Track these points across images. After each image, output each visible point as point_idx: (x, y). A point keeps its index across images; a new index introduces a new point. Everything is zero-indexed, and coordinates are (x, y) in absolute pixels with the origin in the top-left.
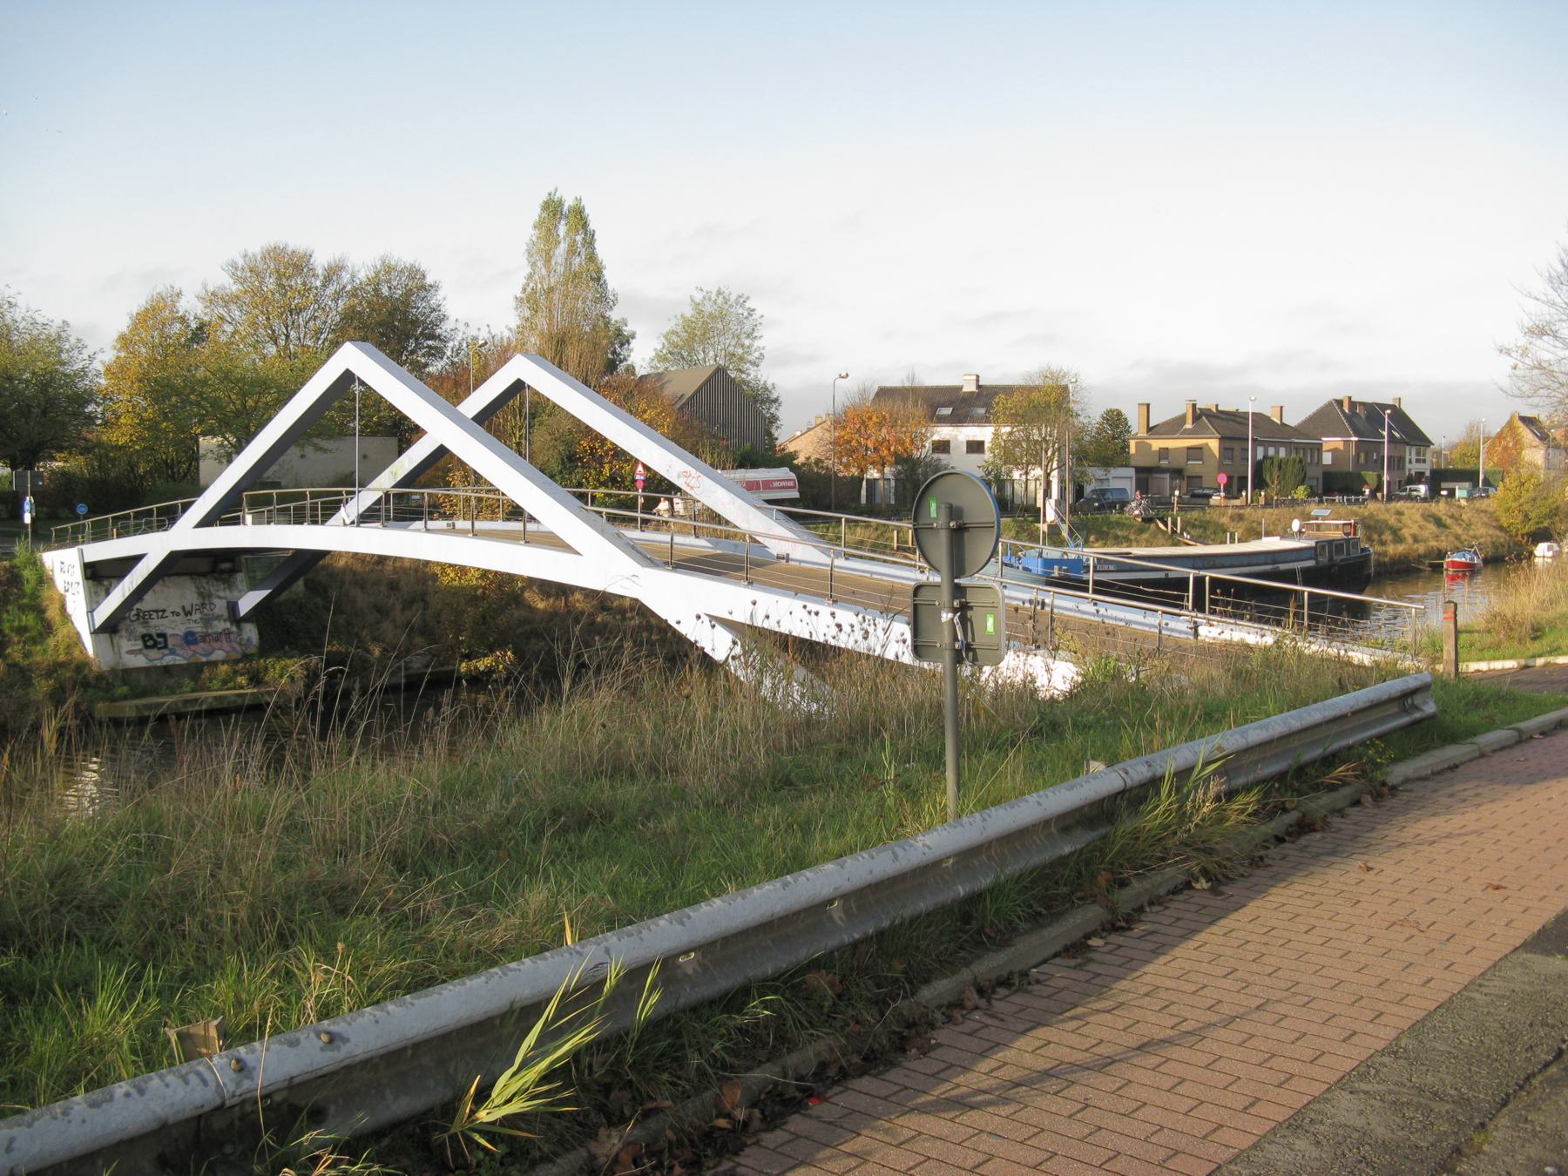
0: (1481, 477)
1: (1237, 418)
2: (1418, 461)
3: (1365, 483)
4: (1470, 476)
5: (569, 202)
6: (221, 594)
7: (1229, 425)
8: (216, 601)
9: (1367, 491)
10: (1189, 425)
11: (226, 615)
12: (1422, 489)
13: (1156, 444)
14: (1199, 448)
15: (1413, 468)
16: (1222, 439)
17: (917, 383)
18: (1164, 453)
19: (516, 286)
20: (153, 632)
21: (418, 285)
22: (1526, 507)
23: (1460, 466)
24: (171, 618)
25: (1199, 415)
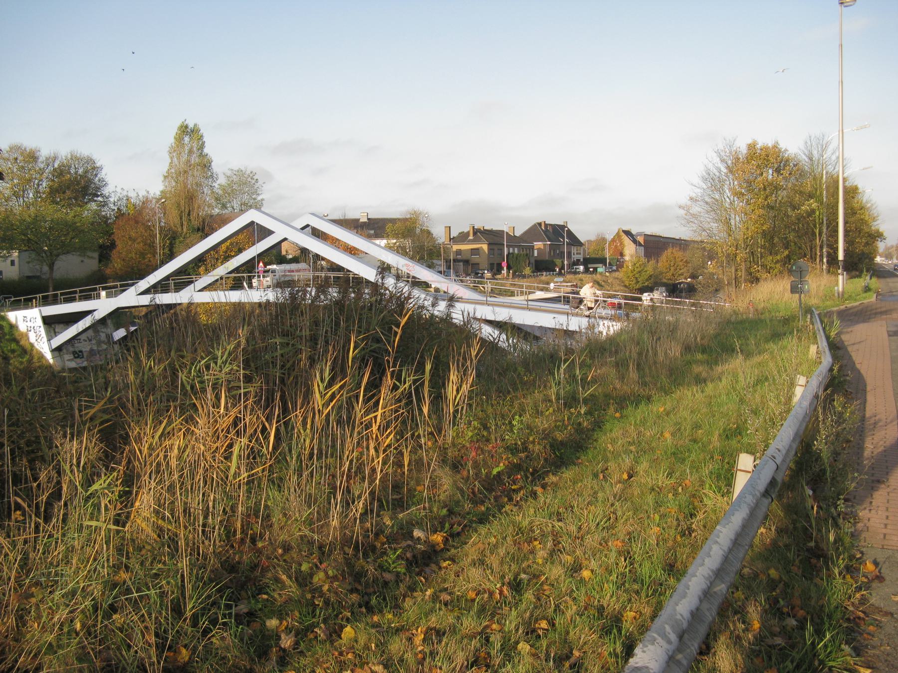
0: (608, 261)
1: (499, 234)
2: (577, 254)
3: (556, 265)
4: (602, 261)
5: (191, 126)
6: (103, 330)
7: (494, 237)
8: (101, 334)
9: (558, 270)
10: (471, 237)
11: (106, 341)
12: (581, 268)
13: (455, 247)
14: (478, 249)
15: (575, 257)
16: (489, 244)
17: (346, 218)
18: (459, 252)
19: (164, 167)
20: (77, 350)
21: (92, 168)
22: (637, 276)
23: (593, 256)
24: (84, 343)
25: (476, 232)
